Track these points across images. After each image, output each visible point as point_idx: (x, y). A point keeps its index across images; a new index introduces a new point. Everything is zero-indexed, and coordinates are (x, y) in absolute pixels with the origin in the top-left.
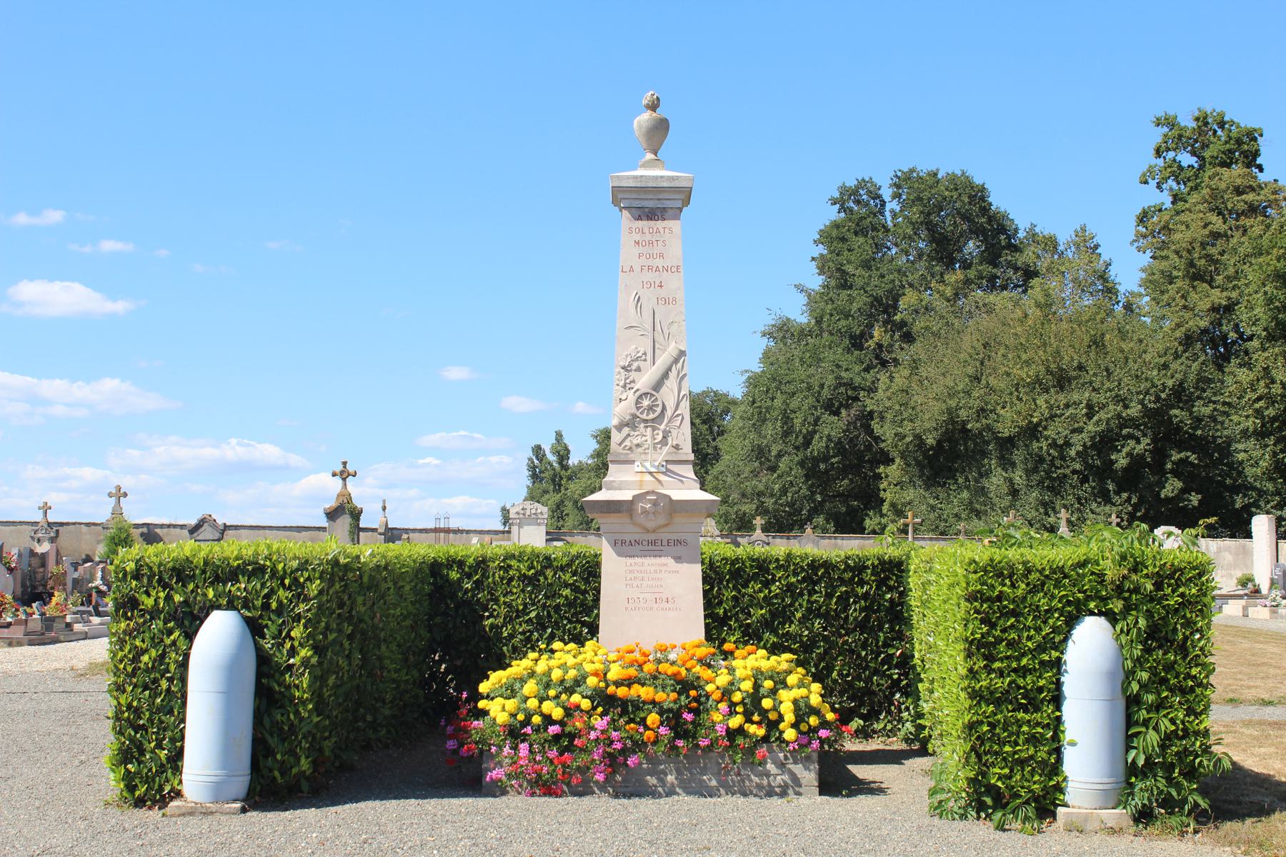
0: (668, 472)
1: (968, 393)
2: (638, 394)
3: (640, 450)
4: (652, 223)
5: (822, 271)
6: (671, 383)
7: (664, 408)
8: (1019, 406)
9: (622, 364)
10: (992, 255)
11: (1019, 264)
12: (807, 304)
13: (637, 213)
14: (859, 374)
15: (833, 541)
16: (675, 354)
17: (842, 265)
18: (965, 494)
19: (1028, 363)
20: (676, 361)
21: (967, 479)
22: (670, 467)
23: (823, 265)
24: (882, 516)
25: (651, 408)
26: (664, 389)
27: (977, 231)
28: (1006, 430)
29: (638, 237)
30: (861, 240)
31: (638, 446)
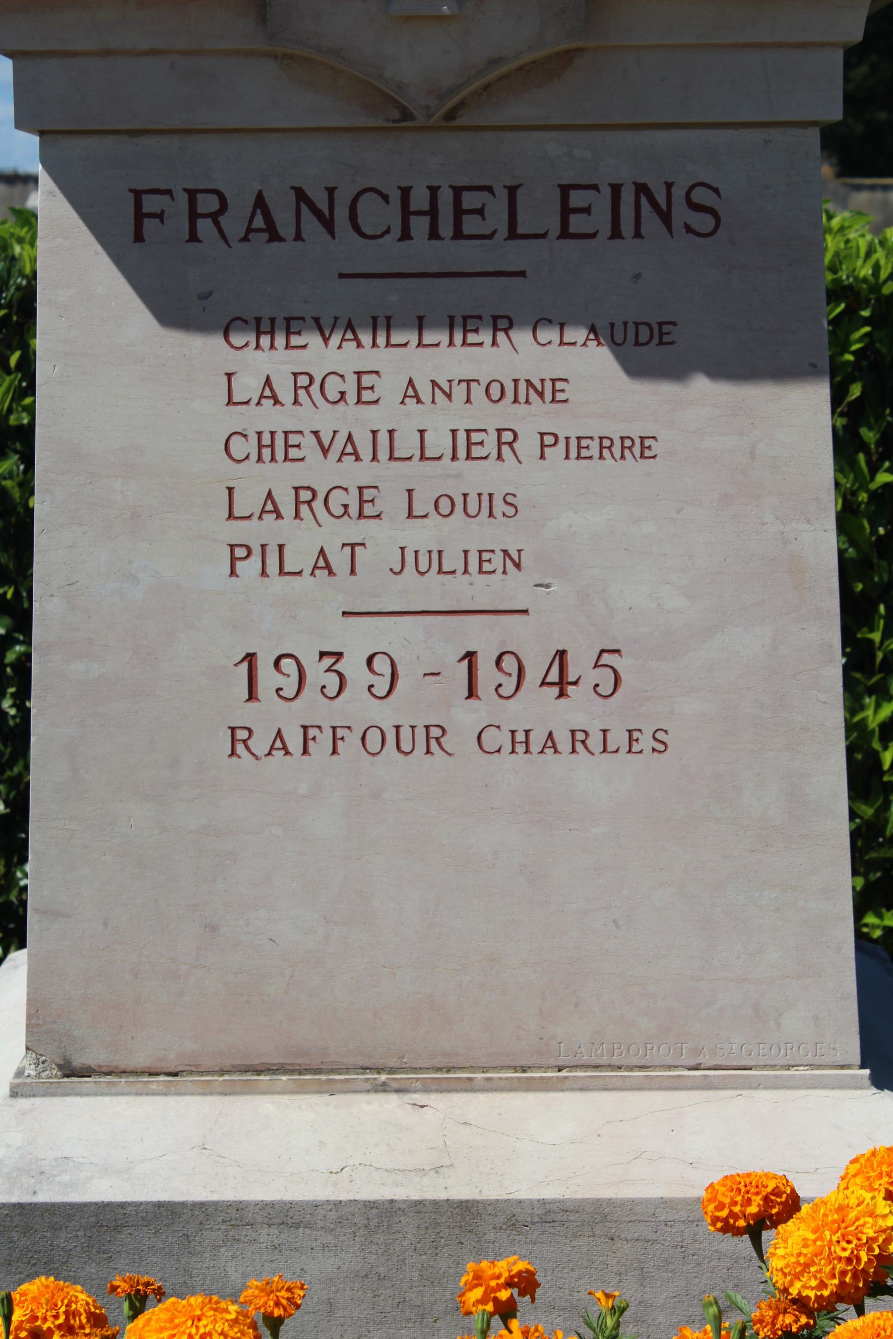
15: (879, 195)
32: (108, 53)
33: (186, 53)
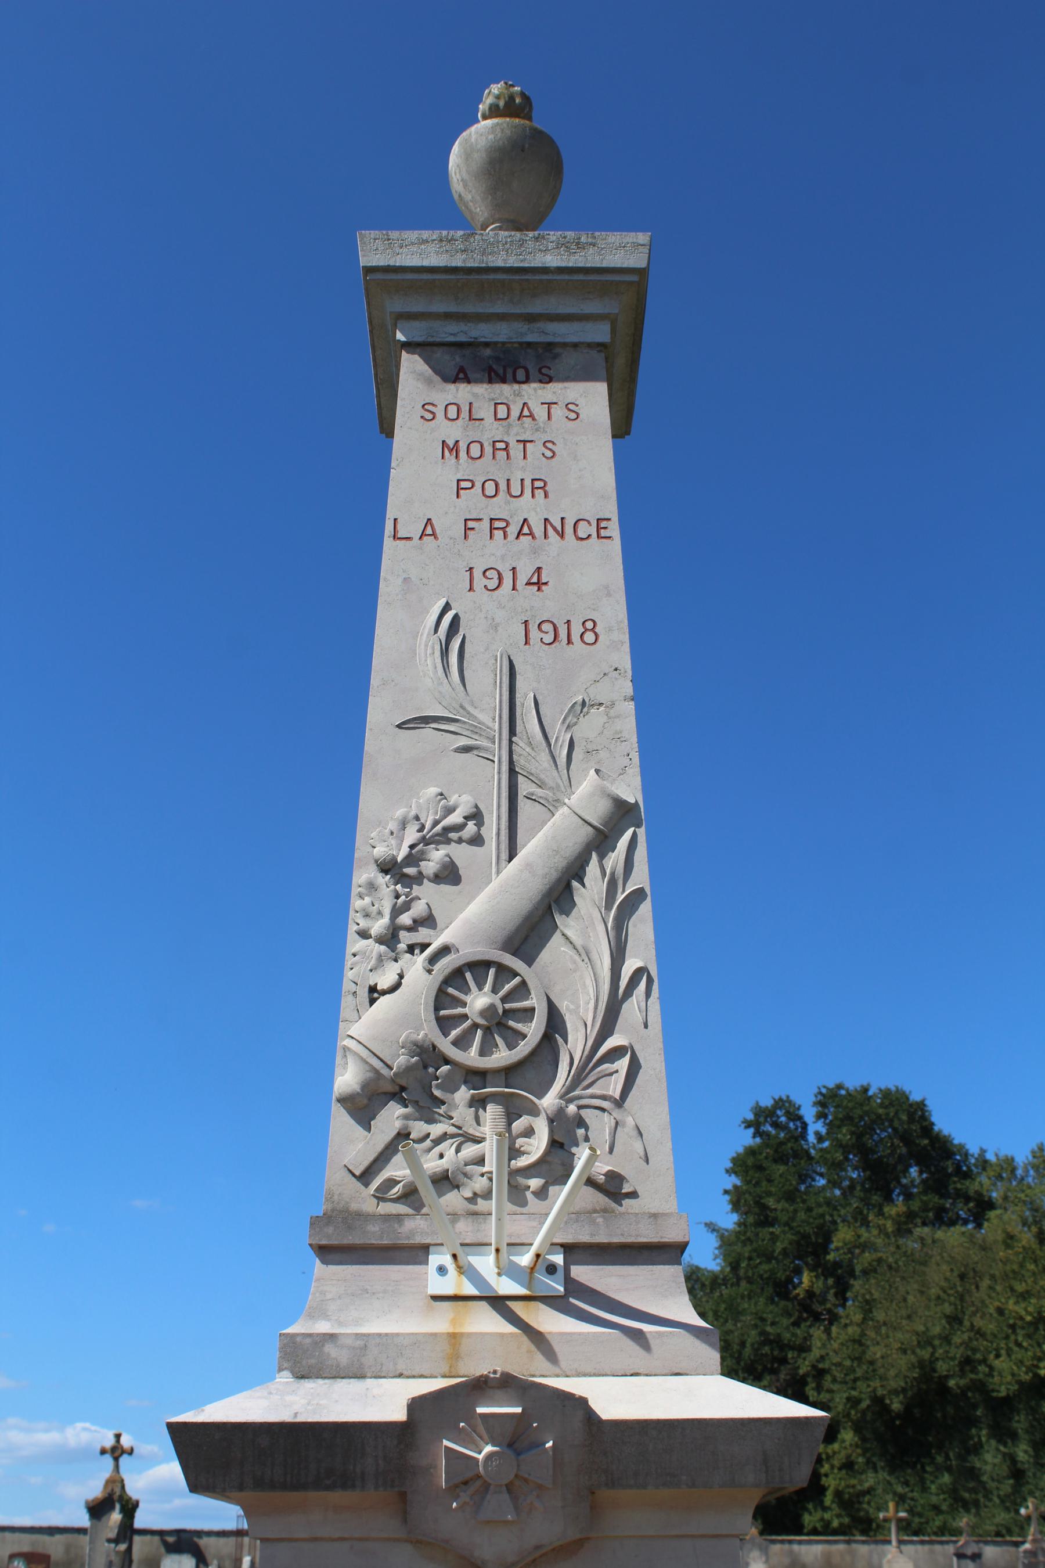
0: (572, 1299)
1: (946, 1339)
2: (446, 965)
3: (453, 1200)
4: (506, 390)
5: (736, 1206)
6: (586, 922)
7: (555, 1024)
8: (1018, 1354)
9: (381, 851)
10: (938, 1184)
11: (971, 1193)
12: (720, 1247)
13: (451, 361)
14: (787, 1328)
15: (786, 1546)
16: (597, 812)
17: (761, 1197)
18: (946, 1478)
19: (1024, 1296)
20: (602, 840)
21: (947, 1458)
22: (582, 1273)
23: (737, 1199)
24: (825, 1509)
25: (499, 1025)
26: (554, 952)
27: (922, 1159)
28: (1003, 1387)
29: (453, 432)
30: (782, 1168)
31: (444, 1181)
32: (315, 1539)
33: (360, 1539)
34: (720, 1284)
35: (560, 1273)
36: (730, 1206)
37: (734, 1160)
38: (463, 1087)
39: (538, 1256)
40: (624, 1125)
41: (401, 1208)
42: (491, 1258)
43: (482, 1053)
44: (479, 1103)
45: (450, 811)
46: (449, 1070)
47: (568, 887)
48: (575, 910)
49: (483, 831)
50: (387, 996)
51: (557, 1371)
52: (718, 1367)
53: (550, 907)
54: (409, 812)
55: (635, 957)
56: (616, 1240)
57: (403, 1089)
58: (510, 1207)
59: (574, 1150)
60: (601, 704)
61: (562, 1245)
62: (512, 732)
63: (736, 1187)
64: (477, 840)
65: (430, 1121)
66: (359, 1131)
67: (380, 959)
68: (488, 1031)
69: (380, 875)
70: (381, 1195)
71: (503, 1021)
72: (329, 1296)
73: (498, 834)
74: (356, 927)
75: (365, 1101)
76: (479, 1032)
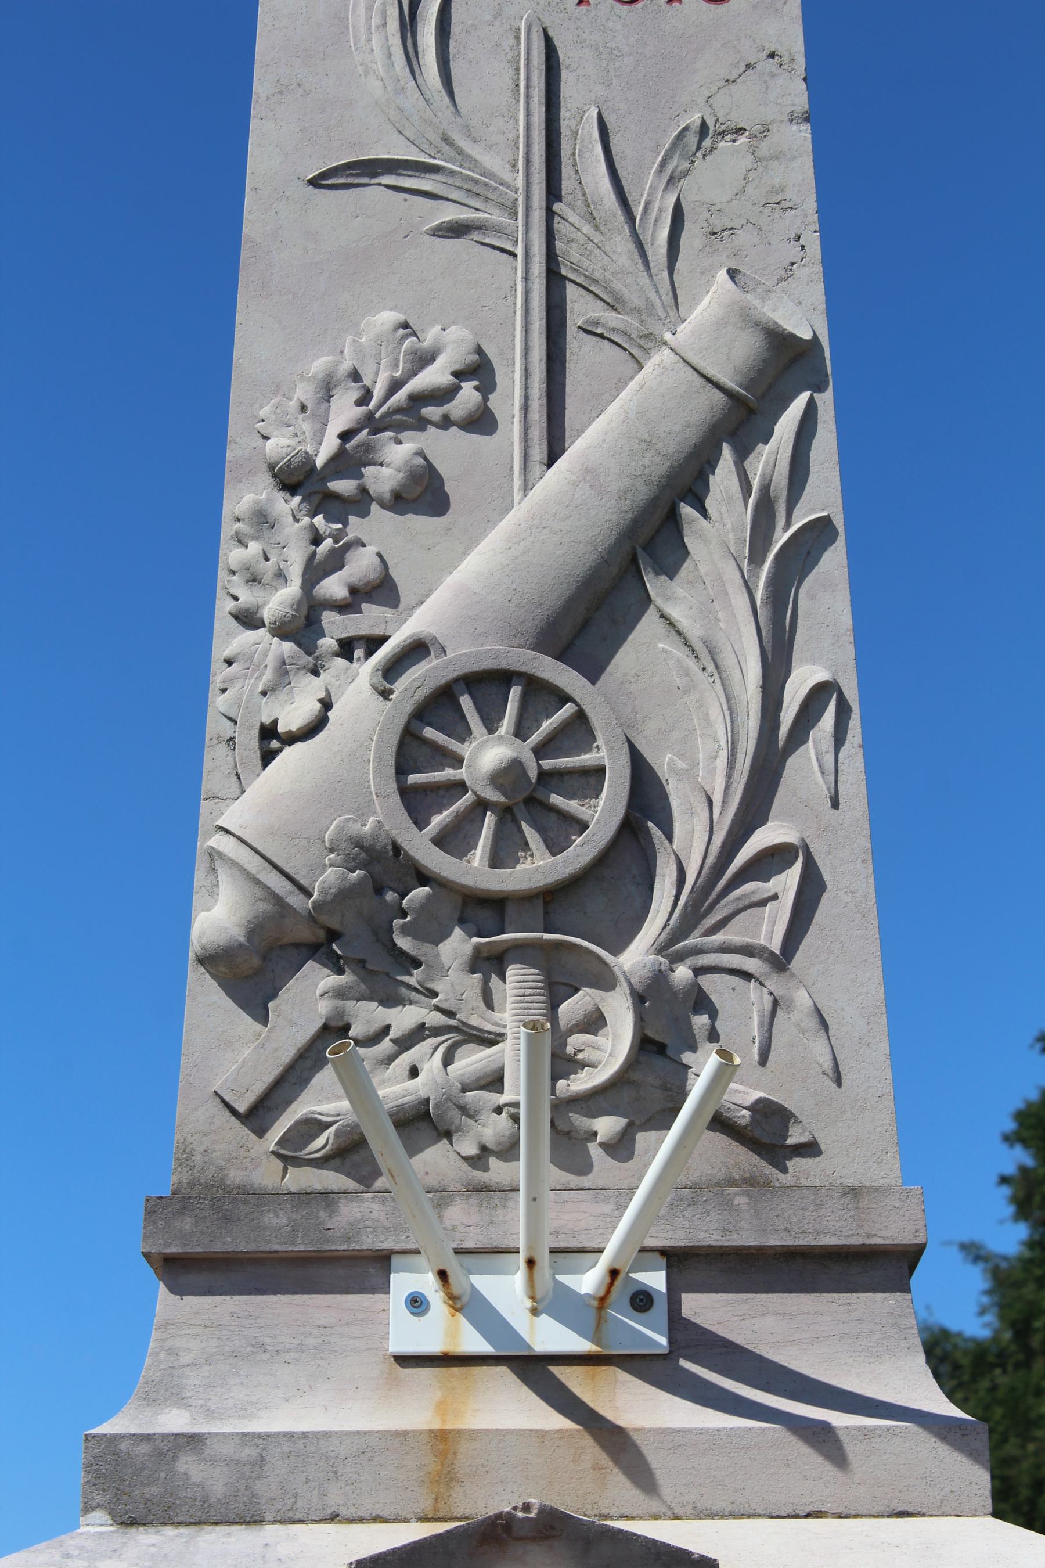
0: (685, 1362)
2: (419, 679)
3: (438, 1161)
6: (710, 590)
9: (280, 445)
12: (989, 1292)
16: (732, 359)
20: (742, 419)
22: (703, 1308)
25: (529, 803)
26: (644, 652)
31: (420, 1123)
34: (993, 1366)
35: (660, 1310)
36: (1011, 1210)
37: (1020, 1116)
38: (458, 932)
39: (614, 1273)
40: (790, 1007)
41: (331, 1179)
42: (518, 1279)
43: (497, 860)
44: (489, 963)
45: (423, 359)
46: (429, 897)
47: (673, 518)
48: (687, 565)
49: (495, 402)
50: (299, 746)
51: (655, 1506)
52: (989, 1508)
53: (634, 560)
54: (338, 363)
55: (813, 661)
56: (774, 1241)
57: (333, 935)
58: (555, 1175)
59: (687, 1057)
60: (740, 131)
61: (663, 1252)
62: (553, 192)
63: (1023, 1170)
64: (481, 422)
65: (391, 1001)
66: (245, 1022)
67: (283, 670)
68: (507, 815)
69: (280, 496)
70: (289, 1155)
71: (539, 795)
72: (186, 1358)
73: (526, 408)
74: (230, 605)
75: (256, 961)
76: (490, 819)
